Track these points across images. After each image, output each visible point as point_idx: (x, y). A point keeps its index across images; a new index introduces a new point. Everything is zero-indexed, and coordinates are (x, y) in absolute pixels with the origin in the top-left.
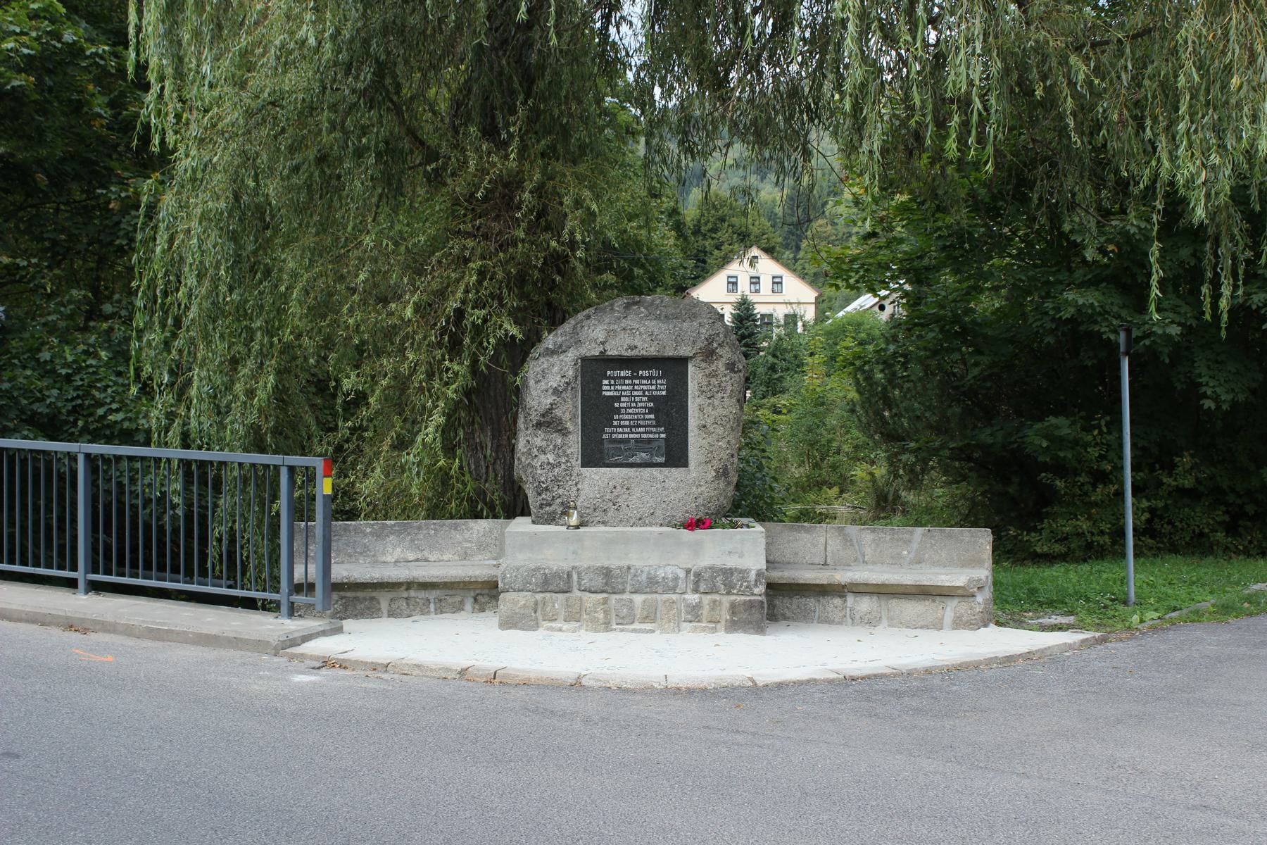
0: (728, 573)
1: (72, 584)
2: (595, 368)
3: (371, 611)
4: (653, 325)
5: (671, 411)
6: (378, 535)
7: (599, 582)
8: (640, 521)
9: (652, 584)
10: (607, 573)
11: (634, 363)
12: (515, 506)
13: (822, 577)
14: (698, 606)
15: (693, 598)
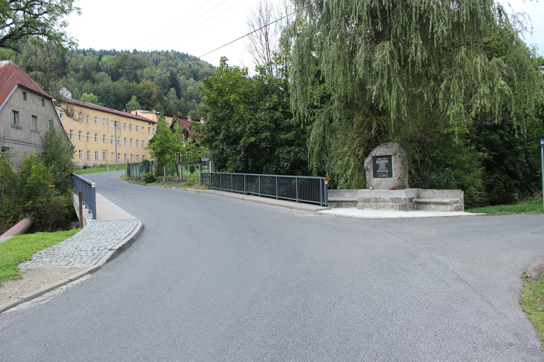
0: (398, 199)
1: (295, 201)
2: (375, 158)
3: (341, 206)
4: (385, 149)
5: (389, 166)
6: (345, 192)
7: (375, 200)
8: (384, 188)
9: (384, 201)
10: (376, 198)
11: (382, 157)
12: (365, 187)
13: (428, 200)
14: (393, 205)
15: (392, 204)
